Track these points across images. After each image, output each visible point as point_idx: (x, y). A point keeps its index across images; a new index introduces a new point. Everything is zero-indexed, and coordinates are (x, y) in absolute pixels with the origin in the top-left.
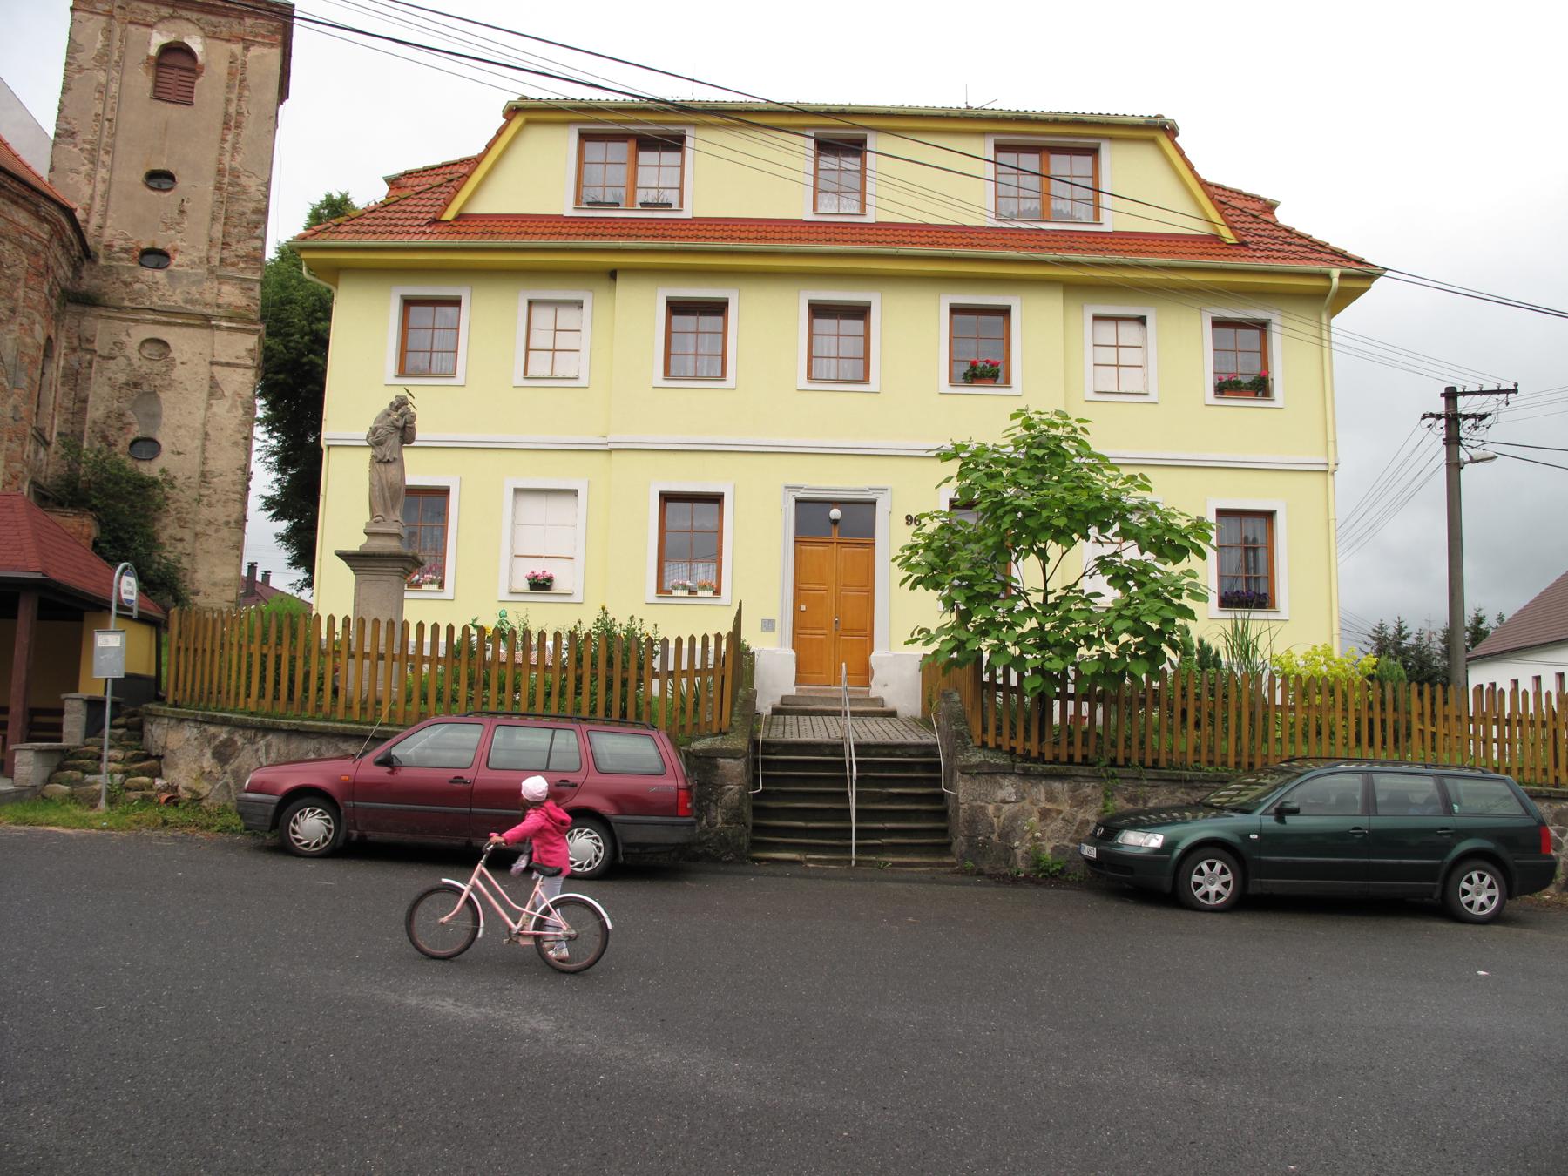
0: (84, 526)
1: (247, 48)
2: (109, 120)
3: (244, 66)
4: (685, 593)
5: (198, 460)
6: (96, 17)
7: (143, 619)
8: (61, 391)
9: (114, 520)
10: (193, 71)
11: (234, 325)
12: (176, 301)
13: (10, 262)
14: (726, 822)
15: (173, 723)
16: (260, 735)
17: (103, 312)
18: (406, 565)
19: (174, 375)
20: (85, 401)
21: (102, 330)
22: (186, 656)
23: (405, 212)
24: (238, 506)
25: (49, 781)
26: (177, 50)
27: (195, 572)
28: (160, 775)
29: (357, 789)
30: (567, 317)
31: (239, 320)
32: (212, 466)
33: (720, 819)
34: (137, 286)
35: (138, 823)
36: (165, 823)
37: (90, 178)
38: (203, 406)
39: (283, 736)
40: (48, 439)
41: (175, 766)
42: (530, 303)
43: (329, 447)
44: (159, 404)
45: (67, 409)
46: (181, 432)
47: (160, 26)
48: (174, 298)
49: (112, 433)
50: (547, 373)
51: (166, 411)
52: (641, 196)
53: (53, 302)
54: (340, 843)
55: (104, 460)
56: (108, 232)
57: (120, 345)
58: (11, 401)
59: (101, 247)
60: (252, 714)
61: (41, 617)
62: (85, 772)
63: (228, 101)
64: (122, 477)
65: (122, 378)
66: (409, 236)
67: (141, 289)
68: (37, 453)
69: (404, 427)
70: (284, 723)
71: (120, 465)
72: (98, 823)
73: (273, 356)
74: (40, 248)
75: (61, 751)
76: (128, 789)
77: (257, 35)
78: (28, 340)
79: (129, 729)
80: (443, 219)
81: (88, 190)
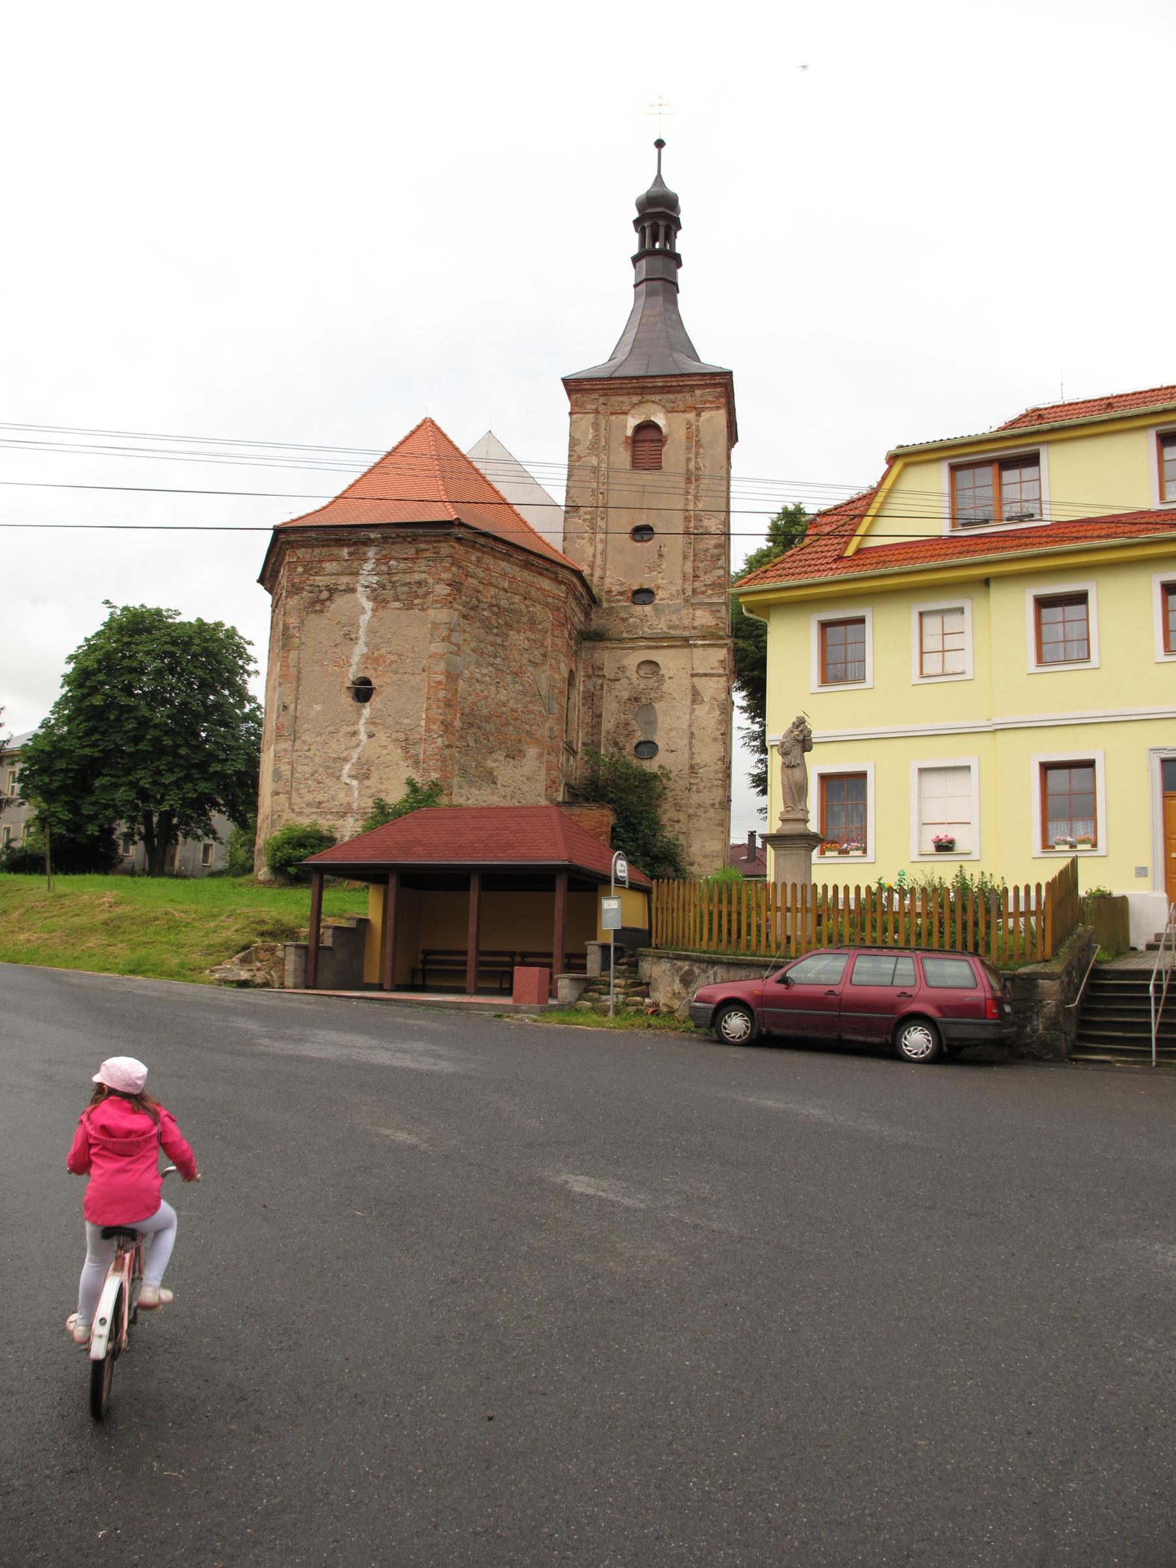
0: (600, 817)
1: (699, 415)
2: (602, 493)
3: (698, 430)
4: (1066, 848)
5: (687, 755)
6: (587, 416)
7: (634, 887)
8: (582, 711)
9: (626, 809)
10: (660, 441)
11: (707, 642)
12: (661, 629)
13: (540, 619)
14: (1046, 1029)
15: (655, 960)
16: (710, 967)
17: (608, 644)
18: (809, 842)
19: (665, 688)
20: (600, 716)
21: (607, 658)
22: (662, 912)
23: (816, 552)
24: (720, 791)
25: (579, 999)
26: (647, 427)
27: (690, 847)
28: (648, 996)
29: (765, 1000)
30: (952, 622)
31: (710, 637)
32: (698, 760)
33: (1041, 1026)
34: (631, 620)
35: (632, 1025)
36: (649, 1026)
37: (592, 541)
38: (688, 711)
39: (725, 967)
40: (575, 748)
41: (656, 990)
42: (921, 614)
43: (772, 746)
44: (655, 712)
45: (588, 724)
46: (673, 734)
47: (633, 411)
48: (660, 626)
49: (621, 739)
50: (939, 671)
51: (660, 718)
52: (1009, 510)
53: (572, 643)
54: (754, 1037)
55: (616, 762)
56: (608, 581)
57: (622, 669)
58: (547, 724)
59: (603, 594)
60: (705, 952)
61: (569, 890)
62: (601, 994)
63: (688, 460)
64: (630, 775)
65: (625, 695)
66: (819, 574)
67: (635, 622)
68: (568, 761)
69: (804, 740)
70: (725, 958)
71: (628, 766)
72: (607, 1025)
73: (747, 656)
74: (560, 604)
75: (586, 980)
76: (628, 1005)
77: (705, 402)
78: (557, 676)
79: (629, 966)
80: (846, 555)
81: (590, 551)
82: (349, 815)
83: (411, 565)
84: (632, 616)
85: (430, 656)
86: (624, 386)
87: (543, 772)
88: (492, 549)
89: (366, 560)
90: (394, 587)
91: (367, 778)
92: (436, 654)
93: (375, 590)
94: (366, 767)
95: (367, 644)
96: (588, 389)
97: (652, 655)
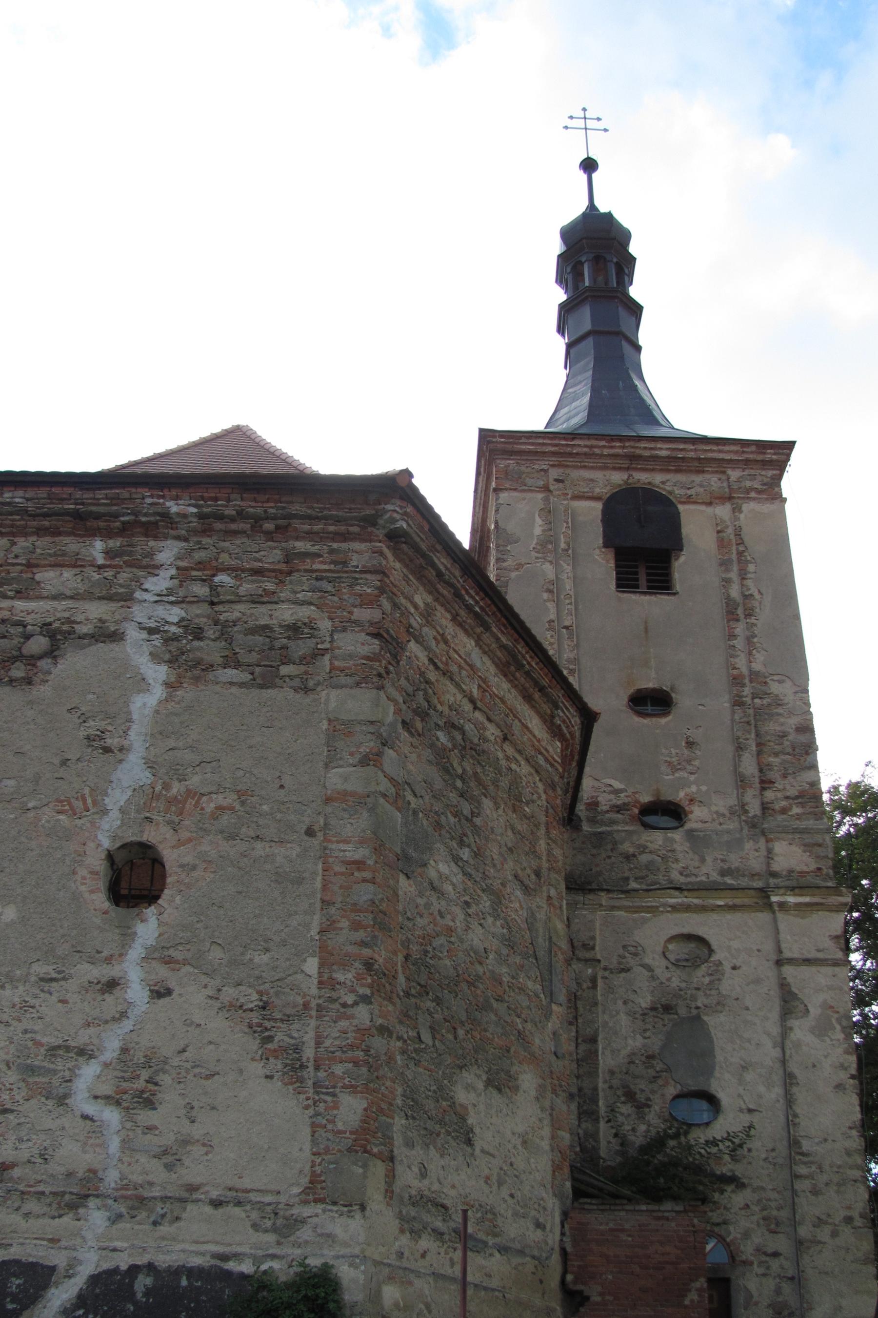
1: (737, 509)
17: (604, 898)
20: (593, 1040)
48: (704, 870)
65: (645, 1001)
67: (651, 862)
82: (92, 1203)
83: (270, 586)
84: (643, 849)
85: (328, 800)
86: (597, 451)
87: (546, 1131)
88: (457, 595)
89: (153, 569)
90: (225, 630)
91: (150, 1104)
92: (345, 793)
93: (176, 638)
94: (145, 1074)
95: (151, 765)
96: (529, 452)
97: (693, 924)
